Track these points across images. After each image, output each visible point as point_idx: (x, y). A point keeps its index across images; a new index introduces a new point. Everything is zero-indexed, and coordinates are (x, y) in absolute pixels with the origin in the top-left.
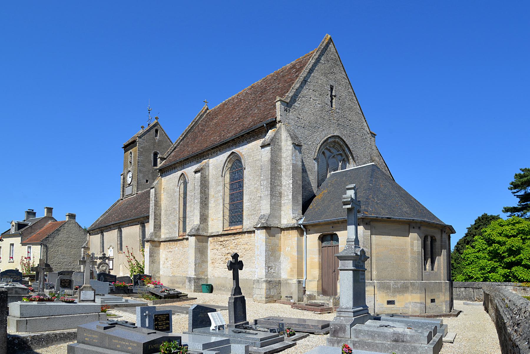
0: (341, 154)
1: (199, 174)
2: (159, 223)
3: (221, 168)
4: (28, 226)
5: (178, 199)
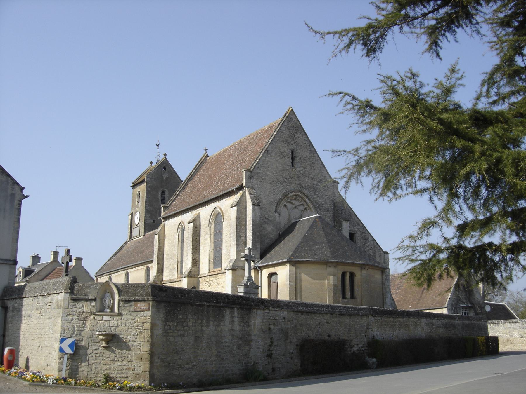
0: (302, 204)
1: (192, 224)
2: (161, 267)
3: (208, 220)
4: (34, 273)
5: (177, 245)
